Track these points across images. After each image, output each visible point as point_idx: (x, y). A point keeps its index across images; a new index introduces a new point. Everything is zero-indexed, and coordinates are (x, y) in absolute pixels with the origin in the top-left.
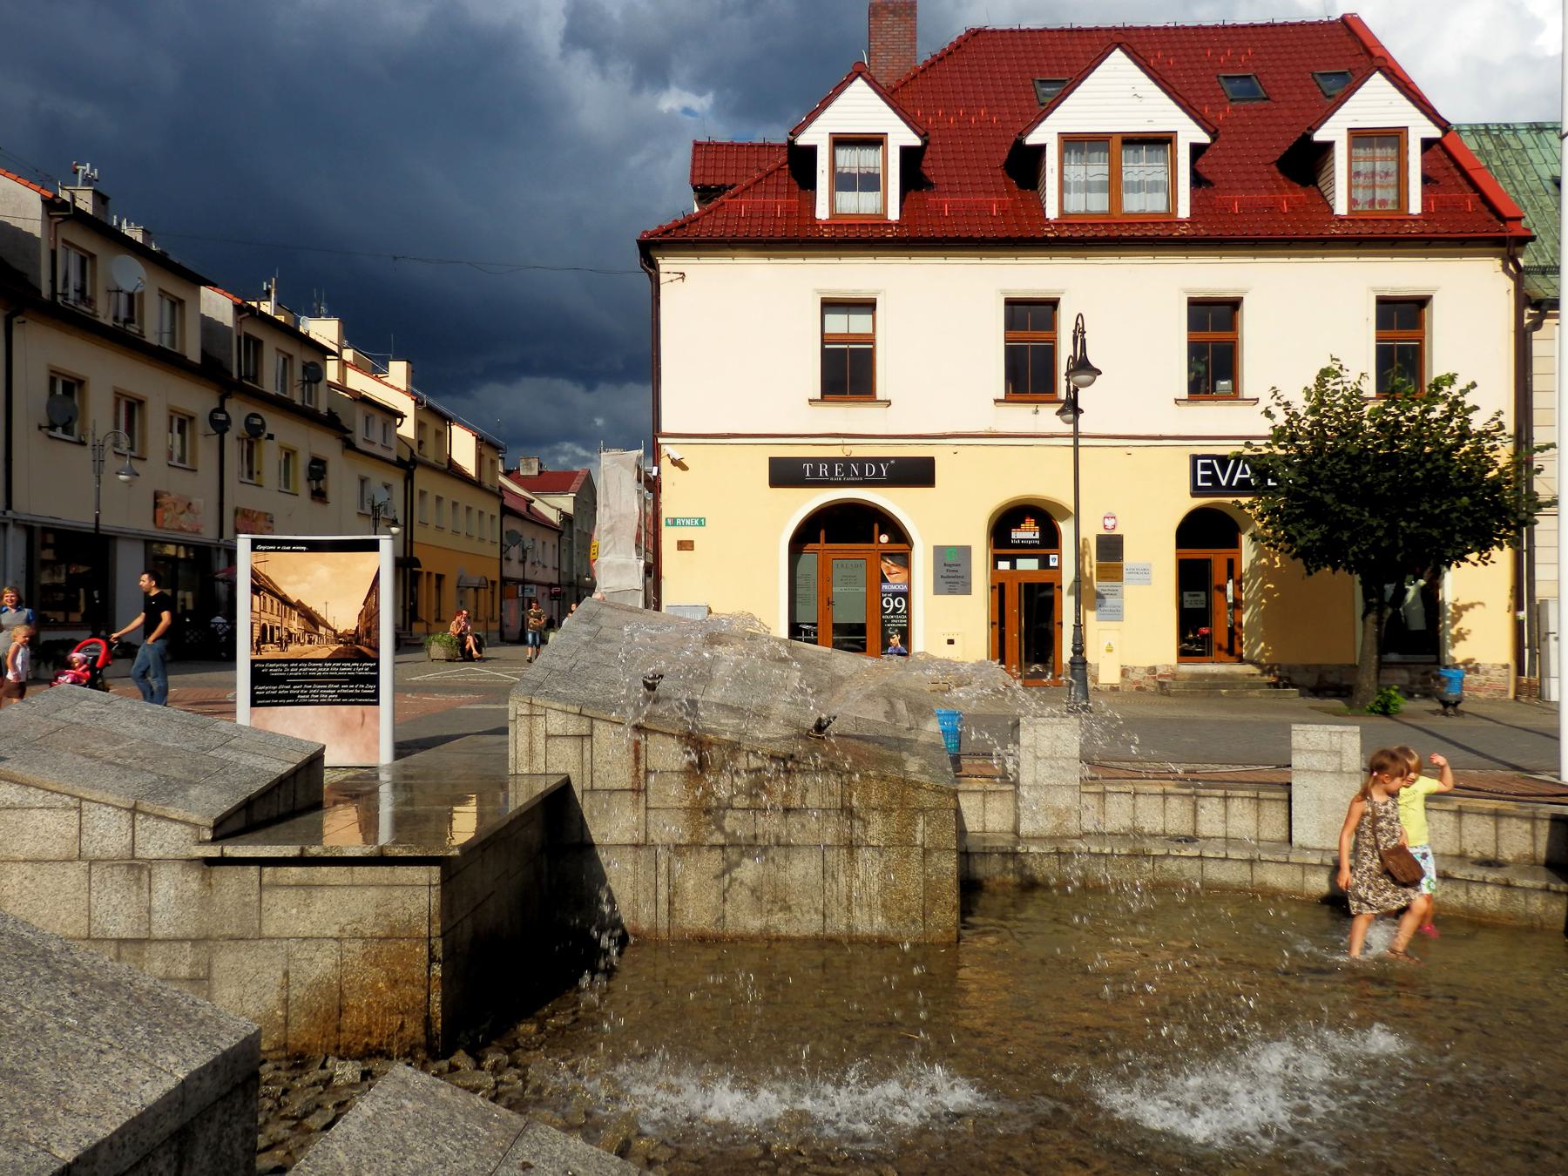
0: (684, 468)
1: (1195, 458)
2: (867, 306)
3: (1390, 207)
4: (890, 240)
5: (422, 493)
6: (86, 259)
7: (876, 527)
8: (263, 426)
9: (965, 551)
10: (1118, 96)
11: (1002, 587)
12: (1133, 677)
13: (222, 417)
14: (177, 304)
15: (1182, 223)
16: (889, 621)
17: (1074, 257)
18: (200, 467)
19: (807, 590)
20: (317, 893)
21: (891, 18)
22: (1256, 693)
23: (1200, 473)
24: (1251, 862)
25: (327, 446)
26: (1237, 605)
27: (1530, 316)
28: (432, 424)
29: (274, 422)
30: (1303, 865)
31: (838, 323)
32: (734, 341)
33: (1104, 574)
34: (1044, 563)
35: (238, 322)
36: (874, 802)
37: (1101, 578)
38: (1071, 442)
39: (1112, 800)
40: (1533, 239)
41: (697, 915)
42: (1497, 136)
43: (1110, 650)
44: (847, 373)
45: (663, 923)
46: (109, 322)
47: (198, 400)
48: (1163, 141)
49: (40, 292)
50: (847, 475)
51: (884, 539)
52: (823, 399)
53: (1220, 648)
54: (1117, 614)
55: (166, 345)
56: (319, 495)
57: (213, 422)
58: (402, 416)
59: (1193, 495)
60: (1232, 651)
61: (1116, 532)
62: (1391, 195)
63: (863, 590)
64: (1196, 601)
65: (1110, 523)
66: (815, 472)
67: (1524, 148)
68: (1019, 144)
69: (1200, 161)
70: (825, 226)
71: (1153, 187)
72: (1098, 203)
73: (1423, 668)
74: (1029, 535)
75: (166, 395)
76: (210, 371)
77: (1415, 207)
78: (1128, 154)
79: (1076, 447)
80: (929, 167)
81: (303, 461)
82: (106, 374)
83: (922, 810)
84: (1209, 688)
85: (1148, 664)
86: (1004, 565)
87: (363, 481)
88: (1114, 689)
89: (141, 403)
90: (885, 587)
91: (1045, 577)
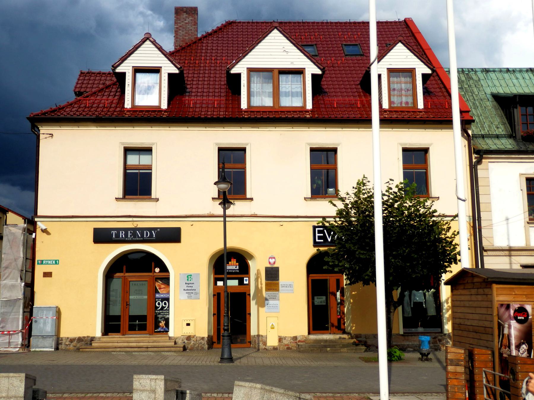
1: (314, 228)
2: (148, 150)
3: (410, 105)
4: (165, 118)
7: (153, 264)
10: (275, 51)
12: (285, 342)
15: (420, 112)
16: (159, 314)
17: (253, 127)
21: (185, 15)
22: (345, 350)
23: (317, 235)
26: (342, 303)
27: (476, 158)
31: (133, 160)
32: (77, 168)
33: (269, 288)
34: (241, 282)
37: (267, 289)
38: (222, 219)
40: (474, 121)
42: (467, 74)
43: (273, 328)
44: (137, 184)
48: (300, 72)
50: (135, 237)
51: (157, 270)
60: (340, 328)
61: (275, 266)
62: (410, 100)
63: (146, 297)
64: (320, 300)
65: (272, 261)
66: (117, 235)
67: (479, 80)
69: (428, 82)
70: (245, 111)
71: (293, 94)
72: (268, 102)
73: (434, 335)
74: (234, 268)
77: (421, 105)
78: (283, 78)
79: (225, 222)
80: (324, 83)
85: (292, 335)
86: (220, 283)
88: (275, 349)
90: (157, 295)
91: (242, 289)
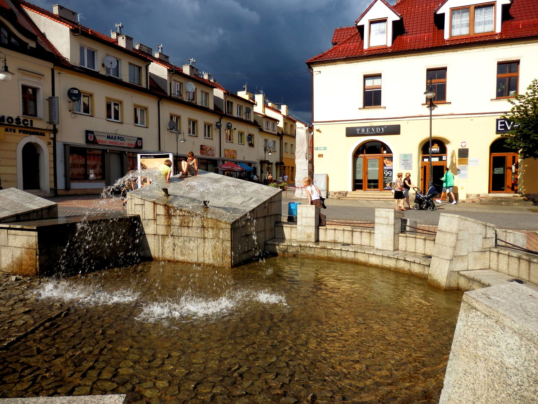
0: (320, 132)
4: (390, 53)
5: (286, 144)
6: (181, 84)
8: (231, 126)
9: (411, 155)
11: (425, 167)
12: (471, 198)
13: (219, 124)
14: (207, 94)
17: (452, 52)
18: (214, 138)
19: (360, 169)
20: (17, 236)
22: (517, 204)
23: (499, 125)
24: (355, 252)
25: (254, 131)
26: (516, 173)
28: (289, 123)
29: (234, 125)
30: (369, 254)
31: (370, 83)
34: (441, 159)
35: (225, 98)
36: (210, 226)
38: (429, 118)
39: (364, 234)
41: (168, 254)
44: (372, 98)
45: (161, 256)
46: (187, 100)
47: (213, 120)
49: (167, 94)
51: (385, 152)
52: (364, 107)
53: (508, 187)
54: (465, 176)
55: (203, 105)
56: (251, 145)
57: (217, 125)
58: (278, 121)
59: (497, 133)
60: (513, 188)
63: (378, 169)
64: (499, 171)
66: (360, 131)
68: (435, 14)
71: (489, 22)
74: (436, 150)
75: (202, 119)
76: (217, 111)
78: (478, 12)
79: (431, 119)
81: (246, 135)
82: (186, 115)
83: (222, 229)
84: (498, 202)
86: (426, 160)
87: (266, 141)
88: (463, 202)
89: (196, 121)
90: (385, 168)
91: (441, 164)
